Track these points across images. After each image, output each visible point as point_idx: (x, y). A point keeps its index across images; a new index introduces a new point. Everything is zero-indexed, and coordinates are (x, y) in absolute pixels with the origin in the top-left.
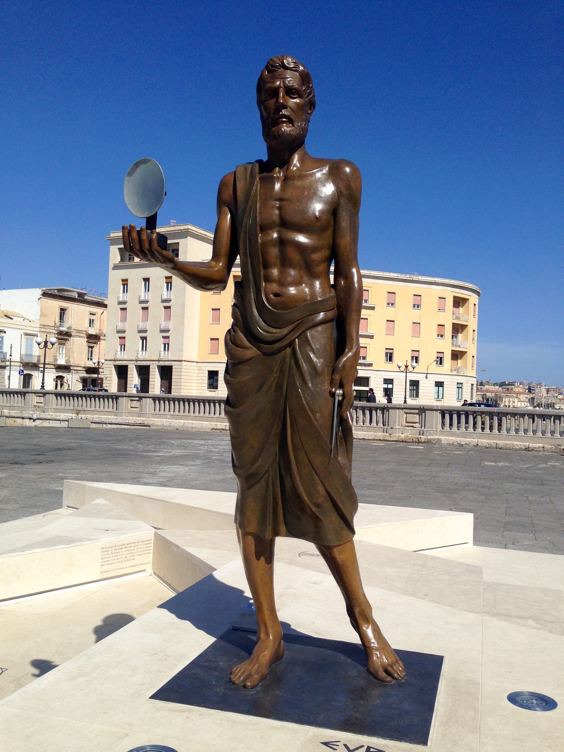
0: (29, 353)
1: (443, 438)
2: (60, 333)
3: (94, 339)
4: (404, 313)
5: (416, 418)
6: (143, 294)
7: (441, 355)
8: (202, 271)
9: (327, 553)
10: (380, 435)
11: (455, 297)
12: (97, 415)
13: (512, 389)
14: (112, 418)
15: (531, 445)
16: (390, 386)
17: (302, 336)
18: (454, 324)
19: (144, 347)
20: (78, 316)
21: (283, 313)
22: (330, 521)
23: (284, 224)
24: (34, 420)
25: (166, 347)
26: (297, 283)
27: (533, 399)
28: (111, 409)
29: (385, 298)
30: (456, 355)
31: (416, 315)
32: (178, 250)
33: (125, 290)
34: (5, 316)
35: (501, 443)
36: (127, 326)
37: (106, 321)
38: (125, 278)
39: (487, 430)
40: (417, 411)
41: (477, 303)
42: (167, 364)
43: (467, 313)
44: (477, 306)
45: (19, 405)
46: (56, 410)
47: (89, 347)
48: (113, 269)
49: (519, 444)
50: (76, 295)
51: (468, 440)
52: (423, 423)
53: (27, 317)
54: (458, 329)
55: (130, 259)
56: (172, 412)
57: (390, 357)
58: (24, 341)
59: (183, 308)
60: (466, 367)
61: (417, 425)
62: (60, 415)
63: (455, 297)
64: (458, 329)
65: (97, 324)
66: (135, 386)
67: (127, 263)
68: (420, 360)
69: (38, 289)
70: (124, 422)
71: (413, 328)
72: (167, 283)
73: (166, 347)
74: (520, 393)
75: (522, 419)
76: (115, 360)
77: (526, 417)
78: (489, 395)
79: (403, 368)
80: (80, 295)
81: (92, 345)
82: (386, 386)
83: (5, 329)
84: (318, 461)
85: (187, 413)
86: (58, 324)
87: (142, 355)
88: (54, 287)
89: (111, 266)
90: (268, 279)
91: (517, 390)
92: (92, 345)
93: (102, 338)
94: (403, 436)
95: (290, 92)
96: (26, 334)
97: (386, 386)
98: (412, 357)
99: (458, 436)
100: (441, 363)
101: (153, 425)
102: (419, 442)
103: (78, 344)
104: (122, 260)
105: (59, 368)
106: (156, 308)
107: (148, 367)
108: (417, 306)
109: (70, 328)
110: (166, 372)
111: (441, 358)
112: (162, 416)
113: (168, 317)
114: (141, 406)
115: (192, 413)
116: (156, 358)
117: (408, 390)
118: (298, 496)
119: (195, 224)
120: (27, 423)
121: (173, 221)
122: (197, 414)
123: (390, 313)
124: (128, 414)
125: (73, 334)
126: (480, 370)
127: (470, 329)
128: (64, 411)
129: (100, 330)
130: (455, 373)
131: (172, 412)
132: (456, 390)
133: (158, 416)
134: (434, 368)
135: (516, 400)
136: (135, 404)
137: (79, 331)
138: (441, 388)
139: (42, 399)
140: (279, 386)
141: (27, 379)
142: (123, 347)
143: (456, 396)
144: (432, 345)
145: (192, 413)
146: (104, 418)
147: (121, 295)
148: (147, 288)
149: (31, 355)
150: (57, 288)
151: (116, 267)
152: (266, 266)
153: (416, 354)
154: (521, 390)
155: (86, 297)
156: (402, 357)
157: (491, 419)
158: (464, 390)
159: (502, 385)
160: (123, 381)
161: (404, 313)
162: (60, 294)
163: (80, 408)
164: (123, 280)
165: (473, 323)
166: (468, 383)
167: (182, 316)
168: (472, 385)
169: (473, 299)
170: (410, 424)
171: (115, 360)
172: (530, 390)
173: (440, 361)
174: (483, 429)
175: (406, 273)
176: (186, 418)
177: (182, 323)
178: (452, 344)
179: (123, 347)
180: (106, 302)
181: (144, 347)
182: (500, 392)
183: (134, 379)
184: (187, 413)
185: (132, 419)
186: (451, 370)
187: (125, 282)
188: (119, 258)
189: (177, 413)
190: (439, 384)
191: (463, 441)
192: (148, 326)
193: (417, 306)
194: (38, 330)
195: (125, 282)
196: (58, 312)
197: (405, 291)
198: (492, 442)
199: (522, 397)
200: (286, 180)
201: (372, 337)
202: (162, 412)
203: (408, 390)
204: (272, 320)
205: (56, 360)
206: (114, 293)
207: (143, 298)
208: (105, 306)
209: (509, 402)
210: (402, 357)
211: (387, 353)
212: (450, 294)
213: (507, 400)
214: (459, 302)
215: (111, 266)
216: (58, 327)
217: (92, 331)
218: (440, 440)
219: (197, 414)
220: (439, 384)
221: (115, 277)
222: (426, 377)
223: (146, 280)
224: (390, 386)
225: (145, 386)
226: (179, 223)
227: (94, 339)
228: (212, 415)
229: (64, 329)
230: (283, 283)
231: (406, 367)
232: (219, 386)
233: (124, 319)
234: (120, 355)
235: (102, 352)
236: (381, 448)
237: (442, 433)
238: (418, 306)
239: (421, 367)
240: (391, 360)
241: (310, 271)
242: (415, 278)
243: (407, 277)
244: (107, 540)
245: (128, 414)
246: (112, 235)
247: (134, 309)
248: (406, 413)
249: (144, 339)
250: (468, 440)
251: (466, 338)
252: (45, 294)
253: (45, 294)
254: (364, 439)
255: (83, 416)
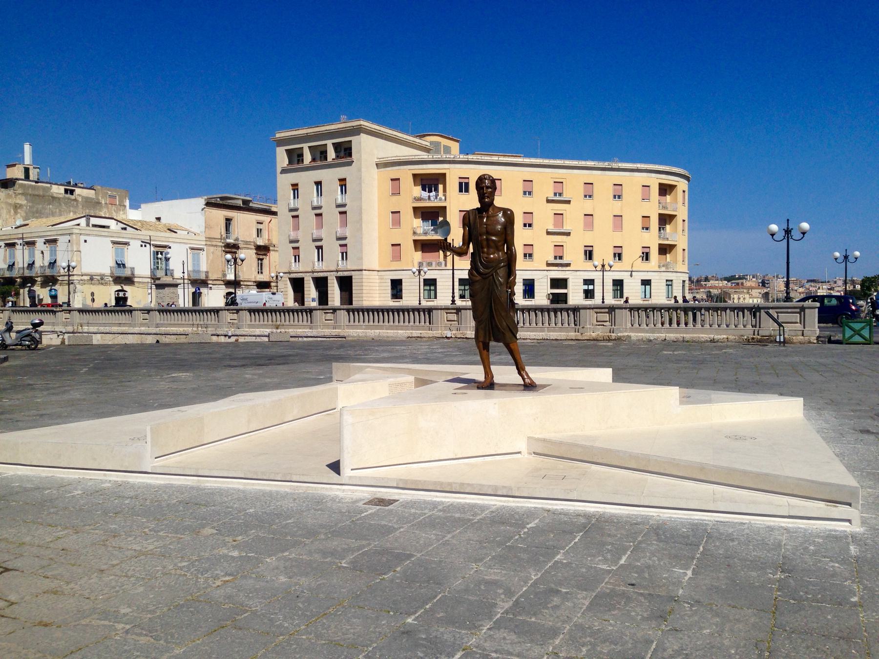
0: (196, 269)
1: (632, 334)
2: (228, 246)
3: (263, 250)
4: (603, 206)
5: (606, 317)
6: (315, 199)
7: (647, 250)
8: (459, 251)
9: (507, 346)
10: (572, 335)
11: (660, 184)
12: (298, 330)
13: (742, 284)
14: (308, 331)
15: (716, 337)
16: (591, 287)
17: (496, 272)
18: (660, 215)
19: (320, 258)
20: (245, 225)
21: (489, 264)
22: (508, 335)
23: (488, 233)
24: (230, 337)
25: (344, 255)
26: (493, 254)
27: (767, 294)
28: (305, 323)
29: (581, 190)
30: (664, 250)
31: (617, 207)
32: (350, 149)
33: (296, 195)
34: (169, 229)
35: (688, 336)
36: (300, 235)
37: (276, 230)
38: (294, 182)
39: (675, 325)
40: (607, 310)
41: (686, 190)
42: (346, 274)
43: (675, 200)
44: (687, 193)
45: (213, 322)
46: (250, 326)
47: (259, 259)
48: (281, 173)
49: (704, 336)
50: (240, 203)
51: (656, 335)
52: (613, 321)
53: (192, 230)
54: (665, 220)
55: (298, 161)
56: (366, 323)
57: (589, 254)
58: (190, 256)
59: (360, 213)
60: (676, 261)
61: (608, 324)
62: (257, 331)
63: (660, 184)
64: (665, 220)
65: (265, 234)
66: (313, 300)
67: (296, 166)
68: (624, 256)
69: (200, 199)
70: (320, 335)
71: (614, 223)
72: (341, 186)
73: (344, 255)
74: (752, 288)
75: (724, 313)
76: (290, 273)
77: (728, 311)
78: (715, 292)
79: (599, 268)
80: (245, 202)
81: (261, 257)
82: (586, 287)
83: (170, 244)
84: (503, 314)
85: (381, 323)
86: (224, 235)
87: (318, 266)
88: (216, 195)
89: (279, 170)
90: (483, 252)
91: (748, 284)
92: (261, 257)
93: (271, 248)
94: (594, 335)
95: (488, 187)
96: (192, 249)
97: (586, 287)
98: (615, 254)
99: (647, 332)
100: (647, 259)
101: (349, 336)
102: (609, 340)
103: (247, 254)
104: (290, 162)
105: (228, 284)
106: (331, 214)
107: (326, 279)
108: (618, 197)
109: (237, 239)
110: (346, 284)
111: (647, 254)
112: (357, 327)
113: (344, 224)
114: (335, 318)
115: (386, 323)
116: (334, 269)
117: (422, 291)
118: (497, 326)
119: (367, 119)
120: (222, 339)
121: (343, 117)
122: (391, 323)
123: (588, 206)
124: (322, 327)
125: (241, 246)
126: (693, 263)
127: (679, 219)
128: (259, 326)
129: (269, 240)
130: (663, 269)
131: (366, 323)
132: (665, 287)
133: (353, 327)
134: (640, 265)
135: (747, 296)
136: (330, 316)
137: (247, 243)
138: (648, 287)
139: (235, 316)
140: (488, 289)
141: (196, 297)
142: (297, 258)
143: (665, 294)
144: (637, 238)
145: (386, 323)
146: (300, 331)
147: (292, 201)
148: (320, 193)
149: (199, 272)
150: (220, 196)
151: (284, 171)
152: (483, 248)
153: (618, 251)
154: (753, 284)
155: (251, 205)
156: (604, 254)
157: (686, 314)
158: (674, 288)
159: (728, 279)
160: (300, 294)
161: (603, 206)
162: (224, 202)
163: (278, 323)
164: (293, 185)
165: (682, 213)
166: (678, 279)
167: (360, 221)
168: (684, 281)
169: (682, 185)
170: (601, 323)
171: (290, 273)
172: (763, 284)
173: (646, 257)
174: (678, 324)
175: (604, 160)
176: (381, 328)
177: (360, 229)
178: (660, 237)
179: (297, 258)
180: (274, 209)
181: (320, 258)
182: (726, 287)
183: (311, 292)
184: (381, 323)
185: (327, 332)
186: (659, 267)
187: (295, 187)
188: (286, 161)
189: (371, 323)
190: (646, 283)
191: (652, 336)
192: (323, 233)
193: (618, 197)
194: (204, 243)
195: (295, 187)
196: (223, 223)
197: (604, 181)
198: (679, 336)
199: (755, 292)
200: (488, 217)
201: (568, 234)
202: (357, 323)
203: (422, 291)
204: (485, 267)
205: (225, 275)
206: (284, 200)
207: (315, 204)
208: (274, 213)
209: (739, 299)
210: (604, 254)
211: (586, 251)
212: (654, 181)
213: (736, 296)
214: (665, 190)
215: (279, 170)
216: (224, 239)
217: (260, 242)
218: (630, 337)
219: (391, 323)
220: (646, 283)
221: (284, 182)
222: (631, 276)
223: (318, 184)
224: (591, 287)
225: (323, 298)
226: (351, 118)
227: (263, 250)
228: (407, 323)
229: (230, 241)
230: (489, 254)
231: (603, 266)
232: (404, 295)
233: (296, 228)
234: (294, 267)
235: (273, 264)
236: (571, 345)
237: (632, 330)
238: (619, 197)
239: (626, 263)
240: (590, 258)
241: (498, 249)
242: (615, 165)
243: (606, 165)
244: (391, 380)
245: (322, 327)
246: (278, 135)
247: (307, 218)
248: (597, 313)
249: (319, 248)
250: (656, 335)
251: (675, 230)
252: (209, 204)
253: (209, 204)
254: (556, 340)
255: (283, 330)
